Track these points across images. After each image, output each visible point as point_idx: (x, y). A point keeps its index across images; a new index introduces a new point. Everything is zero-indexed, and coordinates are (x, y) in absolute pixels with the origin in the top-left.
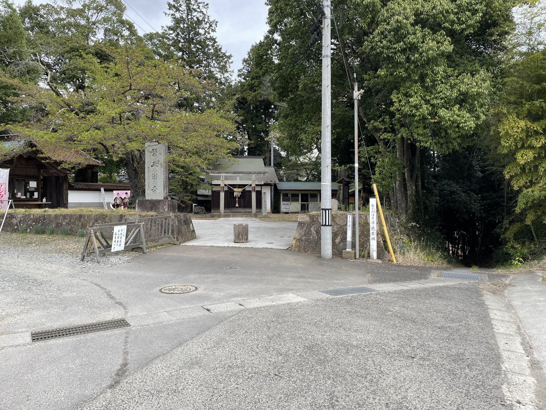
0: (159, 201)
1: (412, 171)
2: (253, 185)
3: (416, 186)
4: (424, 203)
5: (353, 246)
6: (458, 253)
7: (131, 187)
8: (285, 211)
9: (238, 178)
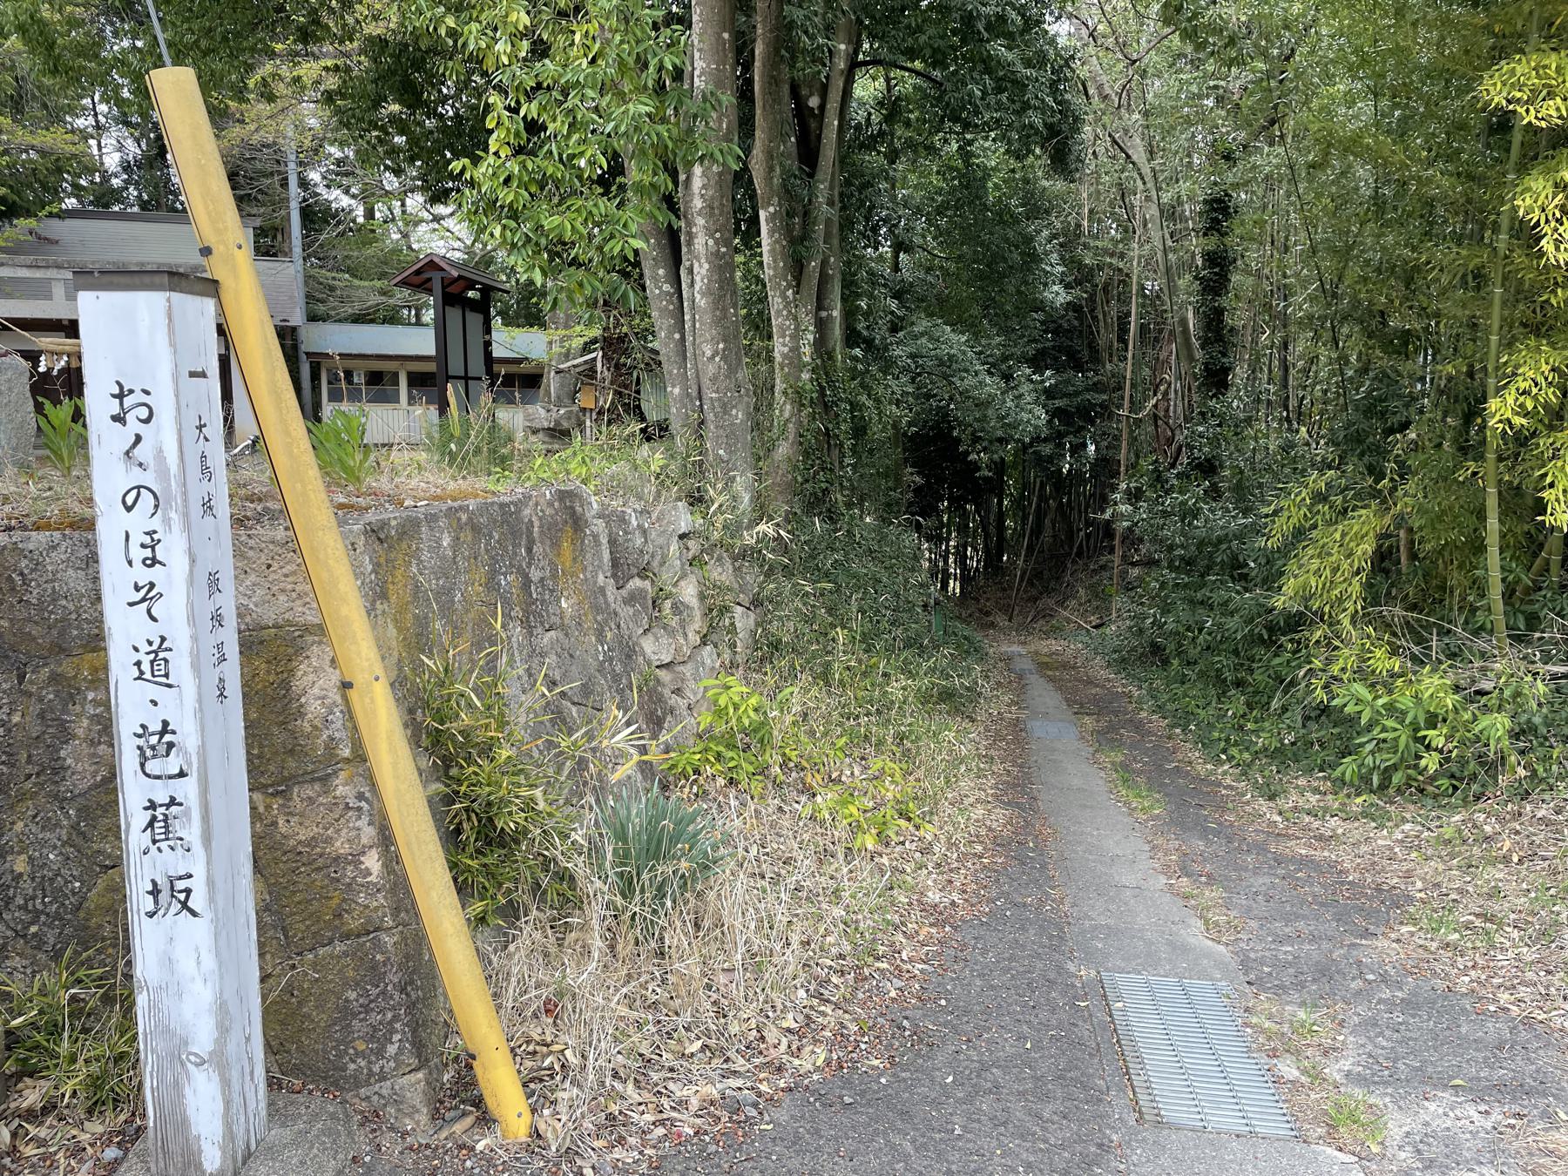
3: (822, 325)
4: (855, 406)
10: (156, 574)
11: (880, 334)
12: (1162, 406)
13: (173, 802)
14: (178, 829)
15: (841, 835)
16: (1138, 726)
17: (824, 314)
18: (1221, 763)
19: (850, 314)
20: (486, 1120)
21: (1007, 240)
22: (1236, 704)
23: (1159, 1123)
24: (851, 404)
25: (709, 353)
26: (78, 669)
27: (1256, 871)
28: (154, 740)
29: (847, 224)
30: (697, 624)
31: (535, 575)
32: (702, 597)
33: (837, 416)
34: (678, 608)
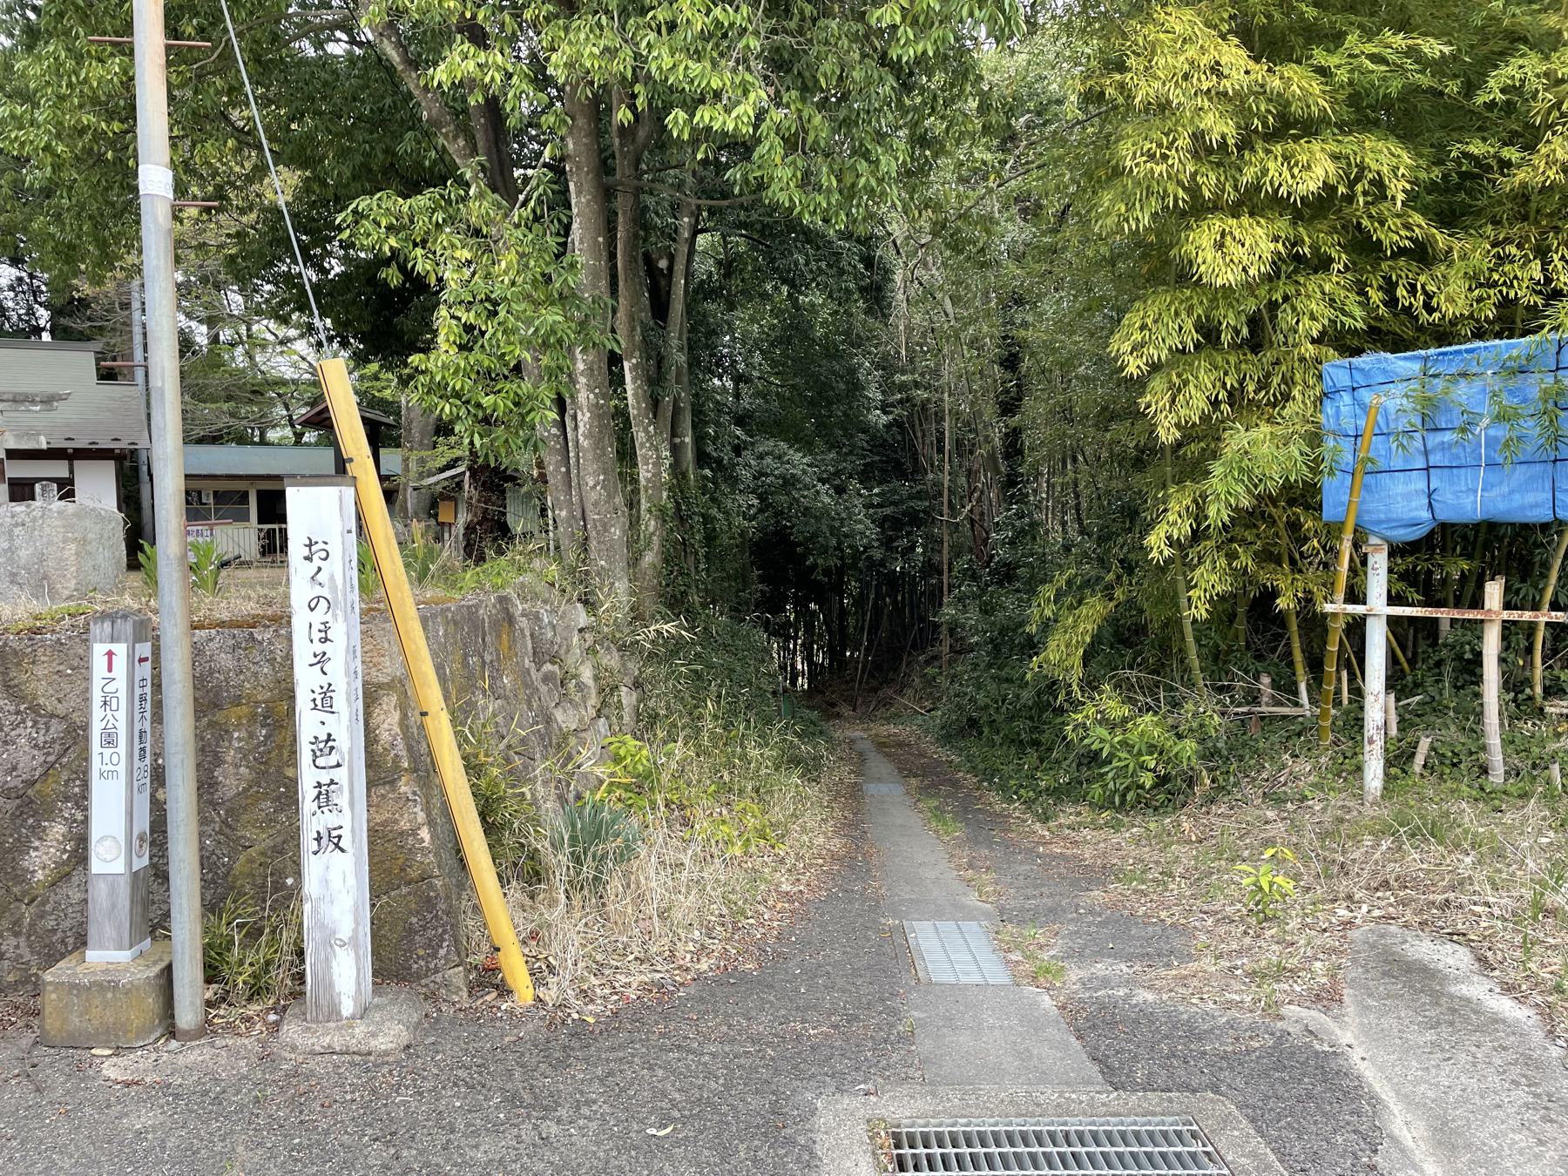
1: (655, 379)
3: (675, 450)
4: (707, 519)
5: (152, 921)
6: (793, 666)
10: (327, 647)
11: (727, 456)
12: (976, 511)
13: (332, 782)
14: (335, 799)
15: (713, 854)
16: (955, 784)
17: (677, 440)
18: (1012, 801)
19: (699, 439)
20: (504, 991)
21: (834, 373)
22: (1033, 755)
23: (930, 983)
24: (703, 515)
25: (591, 483)
26: (228, 718)
27: (1021, 863)
28: (322, 745)
29: (694, 363)
30: (593, 700)
31: (488, 658)
32: (596, 678)
33: (692, 527)
34: (581, 687)
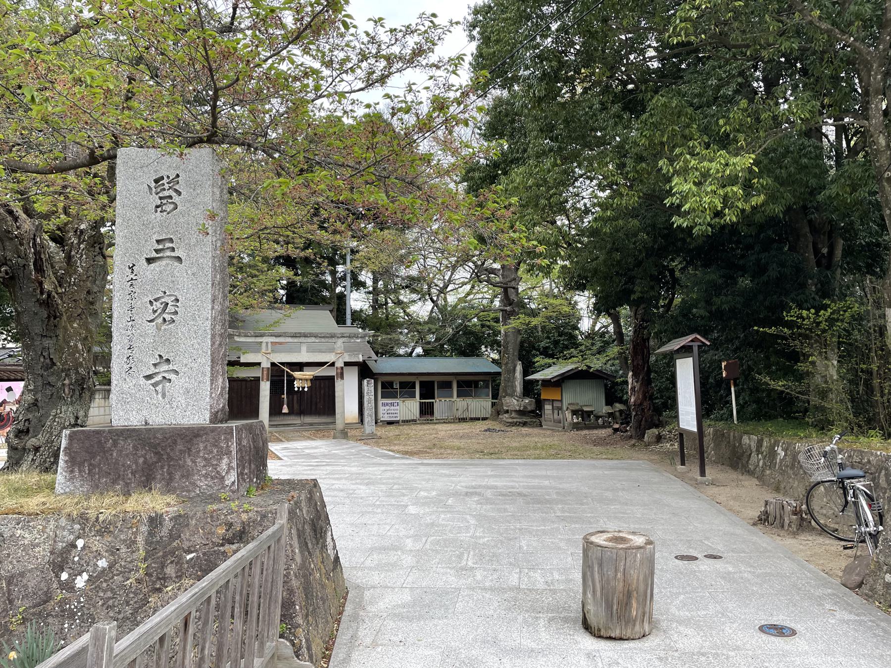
0: (189, 436)
2: (339, 364)
7: (29, 367)
8: (387, 418)
9: (304, 348)
